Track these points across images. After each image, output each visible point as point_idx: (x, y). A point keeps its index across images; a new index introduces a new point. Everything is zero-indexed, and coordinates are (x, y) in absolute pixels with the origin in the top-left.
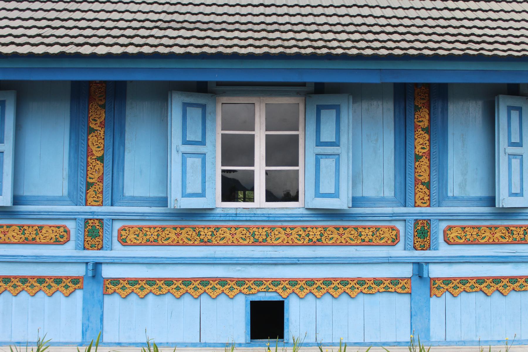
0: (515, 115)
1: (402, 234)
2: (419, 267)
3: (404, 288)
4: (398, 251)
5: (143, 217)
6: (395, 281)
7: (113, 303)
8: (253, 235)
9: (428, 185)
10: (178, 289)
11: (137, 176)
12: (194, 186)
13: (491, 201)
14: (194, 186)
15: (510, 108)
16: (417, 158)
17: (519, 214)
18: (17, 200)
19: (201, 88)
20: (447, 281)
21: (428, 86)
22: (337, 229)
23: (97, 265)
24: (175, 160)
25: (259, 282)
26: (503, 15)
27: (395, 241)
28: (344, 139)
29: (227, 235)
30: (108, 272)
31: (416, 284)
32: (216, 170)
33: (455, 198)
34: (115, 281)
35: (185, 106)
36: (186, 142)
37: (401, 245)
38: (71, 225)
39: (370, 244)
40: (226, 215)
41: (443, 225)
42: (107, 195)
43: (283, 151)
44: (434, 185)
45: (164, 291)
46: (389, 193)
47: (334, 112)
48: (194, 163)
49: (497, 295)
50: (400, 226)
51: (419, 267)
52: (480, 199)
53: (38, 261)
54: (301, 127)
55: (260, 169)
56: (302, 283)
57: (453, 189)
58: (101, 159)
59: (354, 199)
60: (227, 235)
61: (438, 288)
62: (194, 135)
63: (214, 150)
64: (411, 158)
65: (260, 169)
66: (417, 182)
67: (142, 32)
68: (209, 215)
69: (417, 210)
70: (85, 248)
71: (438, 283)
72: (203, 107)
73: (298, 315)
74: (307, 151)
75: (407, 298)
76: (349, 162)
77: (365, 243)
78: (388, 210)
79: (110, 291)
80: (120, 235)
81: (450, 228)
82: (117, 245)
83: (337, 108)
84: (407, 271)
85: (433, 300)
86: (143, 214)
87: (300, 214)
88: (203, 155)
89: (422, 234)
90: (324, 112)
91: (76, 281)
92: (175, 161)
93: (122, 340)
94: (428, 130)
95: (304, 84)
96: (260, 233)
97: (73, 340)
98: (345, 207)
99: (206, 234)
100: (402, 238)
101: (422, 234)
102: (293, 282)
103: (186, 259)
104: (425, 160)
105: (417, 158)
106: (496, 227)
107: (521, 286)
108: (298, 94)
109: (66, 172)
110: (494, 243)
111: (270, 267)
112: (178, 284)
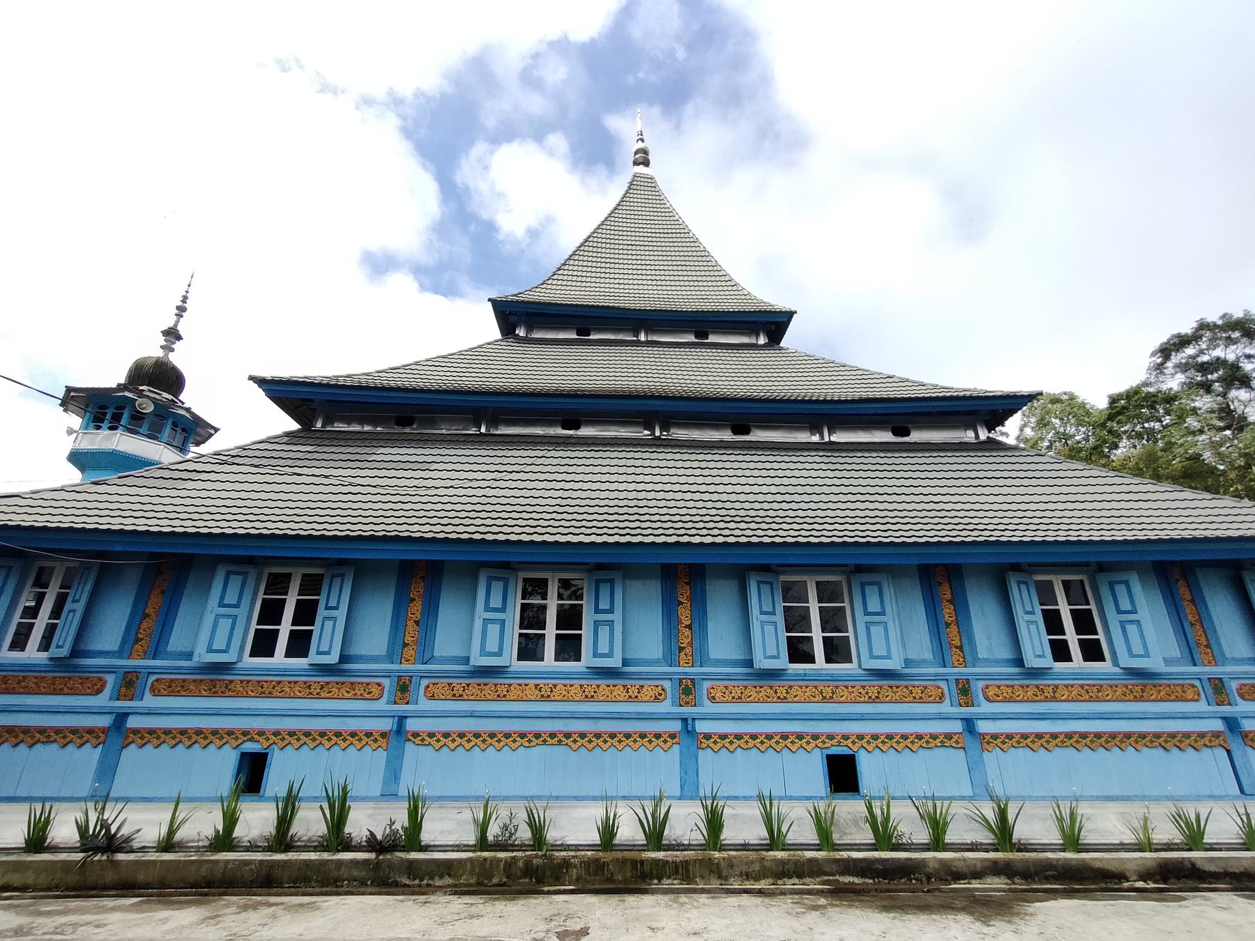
0: (1023, 587)
1: (946, 691)
2: (969, 723)
3: (957, 742)
4: (381, 705)
5: (728, 677)
6: (949, 736)
7: (705, 756)
8: (821, 692)
9: (961, 648)
10: (575, 741)
11: (721, 639)
12: (492, 646)
13: (1019, 662)
14: (772, 651)
15: (1019, 583)
16: (948, 625)
17: (1045, 674)
18: (344, 658)
19: (506, 566)
20: (995, 736)
21: (946, 565)
22: (891, 687)
23: (402, 719)
24: (478, 624)
25: (831, 737)
26: (859, 505)
27: (941, 698)
28: (888, 609)
29: (799, 692)
30: (412, 725)
31: (967, 738)
32: (514, 632)
33: (986, 660)
34: (708, 736)
35: (759, 583)
36: (762, 613)
37: (668, 701)
38: (667, 685)
39: (920, 701)
40: (797, 675)
41: (981, 684)
42: (697, 658)
43: (570, 618)
44: (966, 649)
45: (750, 745)
46: (928, 655)
47: (241, 577)
48: (494, 630)
49: (1042, 750)
50: (943, 684)
51: (969, 723)
52: (1008, 661)
53: (640, 717)
54: (846, 600)
55: (817, 636)
56: (883, 738)
57: (982, 653)
58: (689, 627)
59: (906, 661)
60: (799, 692)
61: (988, 743)
62: (496, 602)
63: (513, 615)
64: (942, 626)
65: (817, 636)
66: (951, 645)
67: (774, 526)
68: (233, 669)
69: (956, 670)
70: (395, 703)
71: (987, 738)
72: (771, 584)
73: (869, 767)
74: (588, 618)
75: (961, 752)
76: (891, 631)
77: (916, 700)
78: (932, 670)
79: (704, 746)
80: (709, 693)
81: (987, 687)
82: (707, 702)
83: (612, 582)
84: (957, 727)
85: (986, 754)
86: (728, 674)
87: (1106, 674)
88: (503, 622)
89: (687, 690)
90: (602, 585)
91: (673, 736)
92: (478, 628)
93: (1216, 793)
94: (951, 602)
95: (846, 565)
96: (828, 691)
97: (373, 794)
98: (898, 667)
99: (502, 690)
100: (947, 696)
101: (687, 690)
102: (860, 737)
103: (763, 713)
104: (954, 628)
105: (948, 625)
106: (1072, 686)
107: (1018, 742)
108: (842, 573)
109: (660, 638)
110: (1028, 701)
111: (848, 721)
112: (500, 736)
